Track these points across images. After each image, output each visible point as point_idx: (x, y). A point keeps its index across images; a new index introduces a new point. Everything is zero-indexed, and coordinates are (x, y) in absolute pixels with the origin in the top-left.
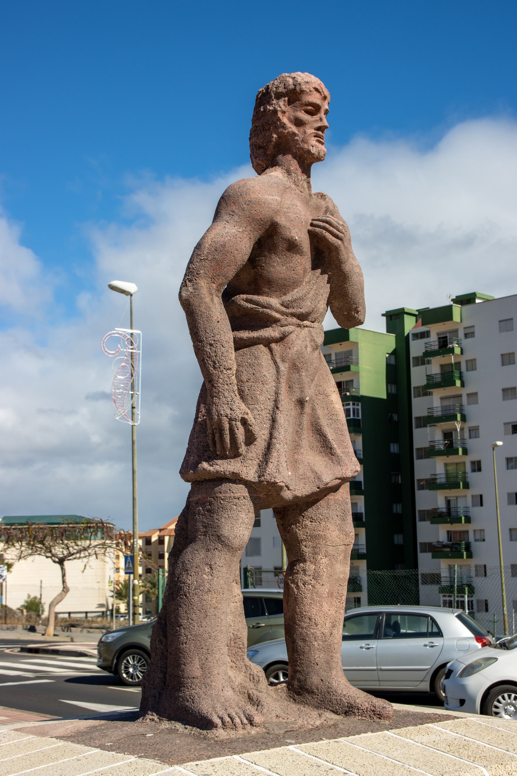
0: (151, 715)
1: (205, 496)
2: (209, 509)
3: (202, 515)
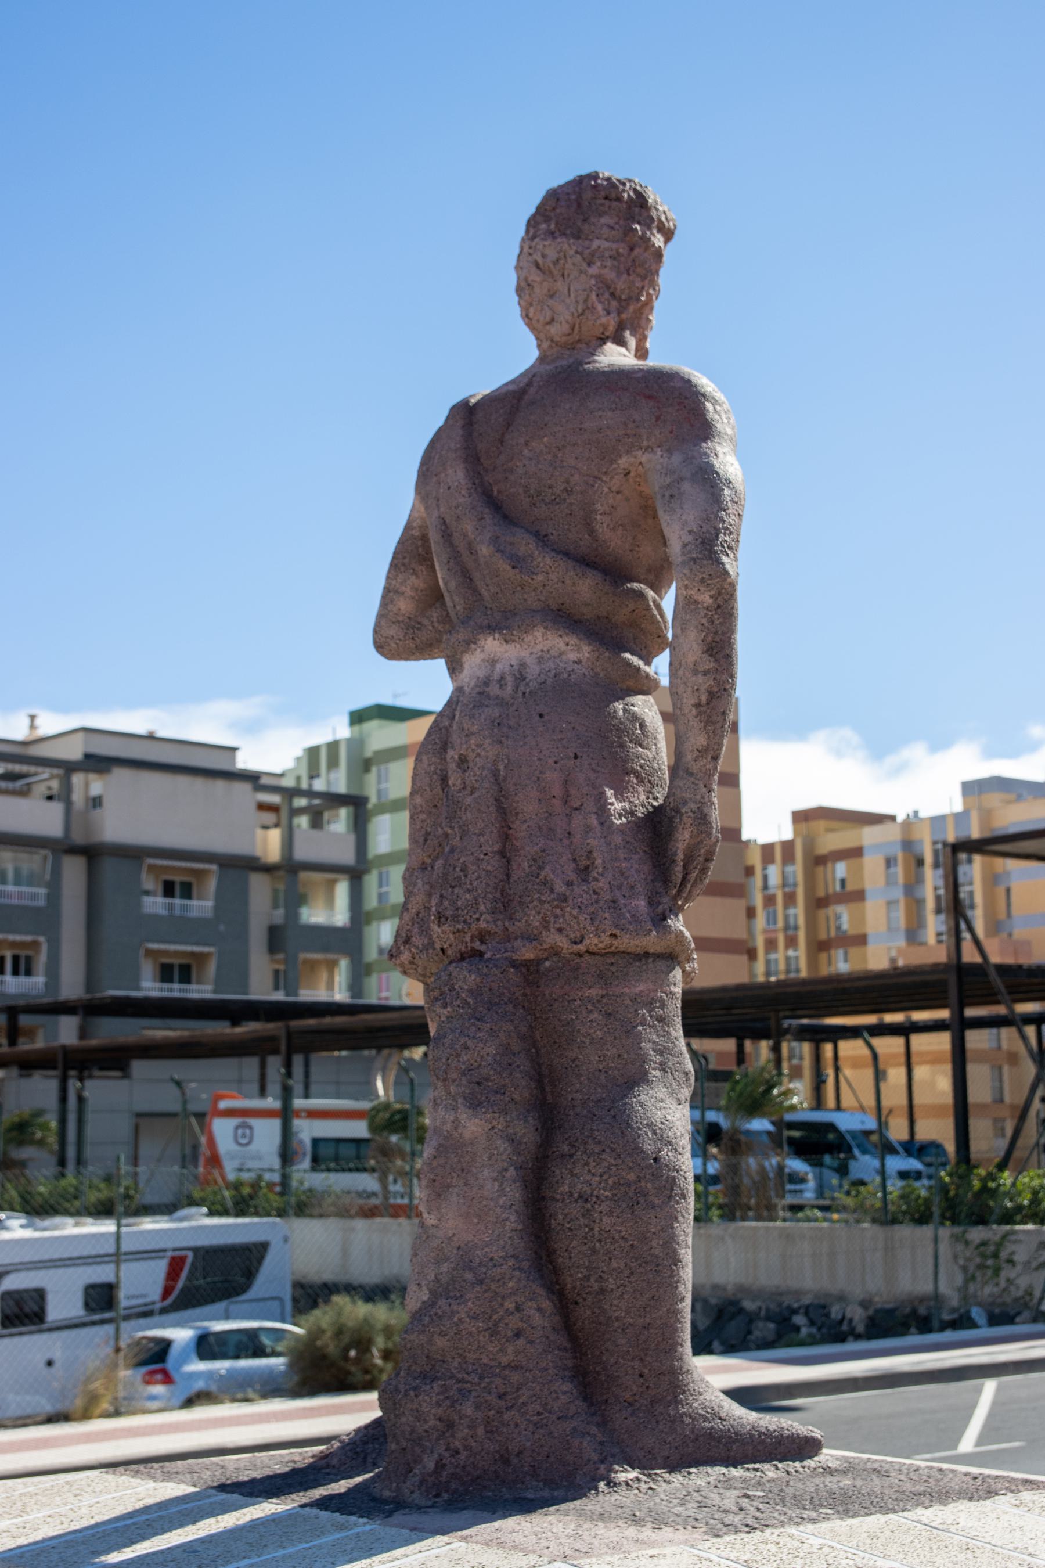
0: (622, 1471)
1: (651, 987)
2: (661, 1016)
3: (650, 1026)
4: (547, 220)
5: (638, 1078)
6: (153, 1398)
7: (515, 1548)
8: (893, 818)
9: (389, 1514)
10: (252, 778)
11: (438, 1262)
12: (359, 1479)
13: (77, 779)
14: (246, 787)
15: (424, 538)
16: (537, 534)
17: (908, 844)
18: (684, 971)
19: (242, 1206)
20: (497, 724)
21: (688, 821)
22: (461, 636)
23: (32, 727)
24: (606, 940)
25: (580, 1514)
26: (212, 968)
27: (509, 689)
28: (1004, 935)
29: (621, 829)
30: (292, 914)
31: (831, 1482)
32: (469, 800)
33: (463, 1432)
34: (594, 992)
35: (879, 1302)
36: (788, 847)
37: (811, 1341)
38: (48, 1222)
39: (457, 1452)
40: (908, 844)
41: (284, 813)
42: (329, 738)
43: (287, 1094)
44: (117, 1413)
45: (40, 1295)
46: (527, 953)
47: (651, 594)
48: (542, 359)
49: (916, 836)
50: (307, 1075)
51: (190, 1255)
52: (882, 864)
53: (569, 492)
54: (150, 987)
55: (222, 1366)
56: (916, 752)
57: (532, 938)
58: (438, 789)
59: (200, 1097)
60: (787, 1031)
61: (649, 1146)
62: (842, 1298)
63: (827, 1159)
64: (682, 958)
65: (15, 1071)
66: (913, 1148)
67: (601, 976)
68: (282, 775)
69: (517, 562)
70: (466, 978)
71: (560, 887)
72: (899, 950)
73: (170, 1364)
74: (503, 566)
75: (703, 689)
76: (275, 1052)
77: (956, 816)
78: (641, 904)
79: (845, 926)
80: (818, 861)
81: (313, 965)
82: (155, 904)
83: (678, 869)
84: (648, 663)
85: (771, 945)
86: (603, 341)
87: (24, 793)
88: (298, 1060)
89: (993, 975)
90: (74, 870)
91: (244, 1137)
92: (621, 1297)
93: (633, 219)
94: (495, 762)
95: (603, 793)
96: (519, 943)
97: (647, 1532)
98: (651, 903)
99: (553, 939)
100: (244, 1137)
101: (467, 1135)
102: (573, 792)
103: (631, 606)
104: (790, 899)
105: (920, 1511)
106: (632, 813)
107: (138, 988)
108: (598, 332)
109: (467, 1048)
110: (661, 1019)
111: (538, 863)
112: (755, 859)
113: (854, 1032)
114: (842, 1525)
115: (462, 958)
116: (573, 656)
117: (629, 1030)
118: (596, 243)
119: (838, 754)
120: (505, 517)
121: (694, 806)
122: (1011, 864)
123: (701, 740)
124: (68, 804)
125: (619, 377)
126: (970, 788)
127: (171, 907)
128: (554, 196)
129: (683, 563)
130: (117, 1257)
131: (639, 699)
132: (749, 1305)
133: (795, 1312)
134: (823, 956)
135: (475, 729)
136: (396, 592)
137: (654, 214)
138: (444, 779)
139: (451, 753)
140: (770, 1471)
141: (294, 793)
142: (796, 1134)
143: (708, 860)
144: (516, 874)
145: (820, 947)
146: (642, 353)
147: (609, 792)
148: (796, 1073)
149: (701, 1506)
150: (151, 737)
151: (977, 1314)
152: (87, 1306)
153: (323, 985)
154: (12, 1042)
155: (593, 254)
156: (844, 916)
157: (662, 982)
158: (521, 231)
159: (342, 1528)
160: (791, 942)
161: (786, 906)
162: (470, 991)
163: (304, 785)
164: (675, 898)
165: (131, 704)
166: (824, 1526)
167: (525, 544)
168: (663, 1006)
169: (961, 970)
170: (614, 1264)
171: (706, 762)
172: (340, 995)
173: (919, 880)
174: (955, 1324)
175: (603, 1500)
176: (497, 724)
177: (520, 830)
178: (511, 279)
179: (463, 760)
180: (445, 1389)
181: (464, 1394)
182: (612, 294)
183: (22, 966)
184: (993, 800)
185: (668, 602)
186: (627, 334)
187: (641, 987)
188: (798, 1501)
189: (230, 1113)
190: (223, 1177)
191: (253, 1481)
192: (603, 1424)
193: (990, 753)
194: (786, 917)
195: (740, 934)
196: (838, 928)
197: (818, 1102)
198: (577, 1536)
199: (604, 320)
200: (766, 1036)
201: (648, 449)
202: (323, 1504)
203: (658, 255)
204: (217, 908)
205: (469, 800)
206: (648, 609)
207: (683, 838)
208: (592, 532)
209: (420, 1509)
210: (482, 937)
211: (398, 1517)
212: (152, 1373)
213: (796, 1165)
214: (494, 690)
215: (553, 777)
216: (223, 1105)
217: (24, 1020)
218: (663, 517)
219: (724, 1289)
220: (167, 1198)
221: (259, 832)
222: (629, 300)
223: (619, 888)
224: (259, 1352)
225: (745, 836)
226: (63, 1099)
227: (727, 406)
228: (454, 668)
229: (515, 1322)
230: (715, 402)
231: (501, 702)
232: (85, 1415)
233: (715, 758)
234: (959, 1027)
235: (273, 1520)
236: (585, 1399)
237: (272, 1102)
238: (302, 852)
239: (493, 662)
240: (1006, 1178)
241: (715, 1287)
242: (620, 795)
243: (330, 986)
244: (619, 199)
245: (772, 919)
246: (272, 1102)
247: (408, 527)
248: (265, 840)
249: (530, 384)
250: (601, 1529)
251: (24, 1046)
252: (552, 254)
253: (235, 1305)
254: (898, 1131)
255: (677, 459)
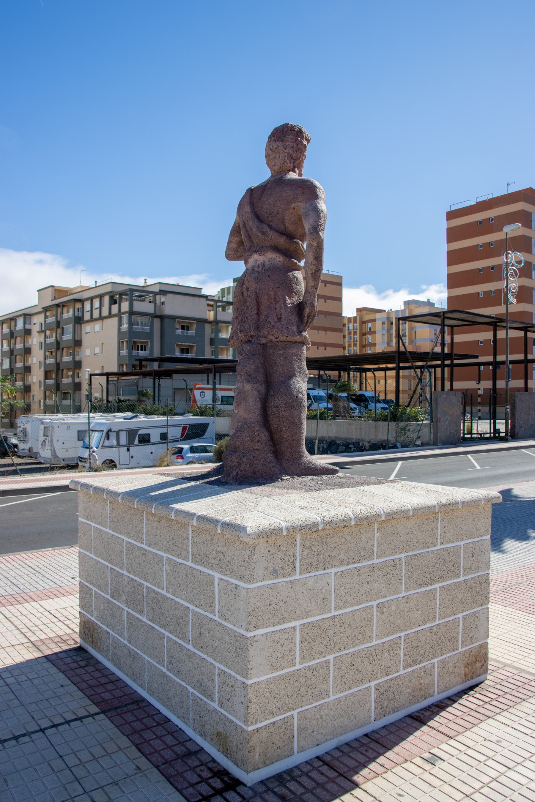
4: (274, 136)
5: (292, 375)
6: (178, 462)
7: (254, 494)
8: (385, 311)
9: (224, 485)
10: (206, 297)
11: (238, 422)
12: (217, 477)
13: (158, 297)
14: (205, 299)
15: (239, 226)
16: (269, 225)
17: (388, 318)
18: (307, 347)
19: (202, 414)
20: (257, 278)
21: (308, 306)
22: (248, 254)
23: (145, 282)
24: (285, 338)
25: (273, 486)
26: (195, 349)
27: (260, 268)
28: (414, 344)
29: (290, 308)
30: (217, 335)
31: (340, 480)
32: (249, 299)
33: (243, 466)
34: (281, 352)
35: (373, 442)
36: (355, 318)
37: (354, 451)
38: (150, 417)
39: (242, 471)
40: (388, 318)
41: (215, 307)
42: (227, 286)
43: (214, 384)
44: (168, 465)
45: (149, 435)
46: (264, 341)
47: (300, 242)
48: (272, 176)
49: (391, 316)
50: (220, 379)
51: (188, 426)
52: (381, 324)
53: (278, 214)
54: (178, 354)
55: (197, 455)
56: (390, 292)
57: (265, 337)
58: (241, 296)
59: (191, 384)
60: (352, 369)
61: (295, 393)
62: (363, 440)
63: (362, 404)
64: (306, 343)
65: (142, 377)
66: (385, 401)
67: (283, 347)
68: (214, 296)
69: (263, 233)
70: (247, 348)
71: (273, 323)
72: (385, 348)
73: (183, 454)
74: (259, 234)
75: (313, 269)
76: (211, 372)
77: (402, 310)
78: (295, 328)
79: (370, 341)
80: (363, 323)
81: (222, 349)
82: (179, 332)
83: (306, 319)
84: (300, 262)
85: (350, 346)
86: (289, 171)
87: (143, 301)
88: (217, 375)
89: (408, 354)
90: (157, 322)
91: (203, 395)
92: (286, 433)
93: (298, 136)
94: (256, 289)
95: (285, 298)
96: (261, 338)
97: (289, 491)
98: (298, 328)
99: (271, 337)
100: (203, 395)
101: (246, 389)
102: (277, 297)
103: (295, 246)
104: (355, 333)
105: (362, 487)
106: (293, 303)
107: (175, 355)
108: (288, 168)
109: (246, 366)
110: (300, 360)
111: (267, 316)
112: (346, 322)
113: (369, 370)
114: (340, 490)
115: (246, 342)
116: (278, 260)
117: (291, 362)
118: (287, 143)
119: (368, 292)
120: (260, 220)
121: (310, 302)
122: (417, 324)
123: (313, 284)
124: (155, 304)
125: (293, 181)
126: (406, 303)
127: (184, 333)
128: (276, 130)
129: (309, 234)
130: (167, 426)
131: (296, 272)
132: (338, 442)
133: (350, 444)
134: (364, 349)
135: (251, 280)
136: (231, 242)
137: (304, 135)
138: (243, 293)
139: (244, 286)
140: (324, 477)
141: (216, 301)
142: (354, 397)
143: (314, 317)
144: (261, 320)
145: (363, 346)
146: (300, 175)
147: (287, 298)
148: (355, 381)
149: (305, 485)
150: (178, 285)
151: (398, 444)
152: (161, 439)
153: (225, 355)
154: (141, 369)
155: (286, 146)
156: (370, 338)
157: (300, 349)
158: (267, 140)
159: (211, 488)
160: (355, 345)
161: (354, 335)
162: (248, 351)
163: (221, 299)
164: (305, 327)
165: (170, 276)
166: (336, 490)
167: (266, 228)
168: (300, 356)
169: (399, 353)
170: (285, 424)
171: (314, 290)
172: (230, 358)
173: (391, 328)
174: (392, 448)
175: (280, 483)
176: (257, 278)
177: (263, 307)
178: (264, 153)
179: (247, 288)
180: (239, 455)
181: (244, 456)
182: (292, 158)
183: (143, 348)
184: (413, 306)
185: (305, 246)
186: (296, 169)
187: (295, 351)
188: (330, 485)
189: (199, 389)
190: (197, 405)
191: (190, 477)
192: (281, 465)
193: (411, 293)
194: (354, 338)
195: (341, 342)
196: (368, 341)
197: (361, 389)
198: (271, 491)
199: (289, 165)
200: (346, 371)
201: (300, 202)
202: (207, 483)
203: (305, 147)
204: (196, 333)
205: (249, 299)
206: (300, 247)
207: (307, 310)
208: (284, 225)
209: (232, 484)
210: (252, 336)
211: (226, 486)
212: (178, 456)
213: (353, 406)
214: (256, 269)
215: (272, 293)
216: (197, 386)
217: (144, 363)
218: (304, 221)
219: (331, 437)
220: (182, 411)
221: (208, 312)
222: (296, 160)
223: (289, 324)
224: (207, 452)
225: (344, 315)
226: (154, 384)
227: (323, 190)
228: (246, 263)
229: (258, 438)
230: (319, 189)
231: (258, 272)
232: (160, 466)
233: (317, 289)
234: (398, 369)
235: (194, 486)
236: (276, 458)
237: (210, 386)
238: (220, 318)
239: (256, 261)
240: (408, 409)
241: (329, 437)
242: (290, 298)
243: (227, 355)
244: (294, 131)
245: (349, 338)
246: (210, 386)
247: (235, 223)
248: (209, 314)
249: (268, 183)
250: (278, 490)
251: (144, 370)
252: (275, 146)
253: (200, 439)
254: (382, 397)
255: (308, 204)
